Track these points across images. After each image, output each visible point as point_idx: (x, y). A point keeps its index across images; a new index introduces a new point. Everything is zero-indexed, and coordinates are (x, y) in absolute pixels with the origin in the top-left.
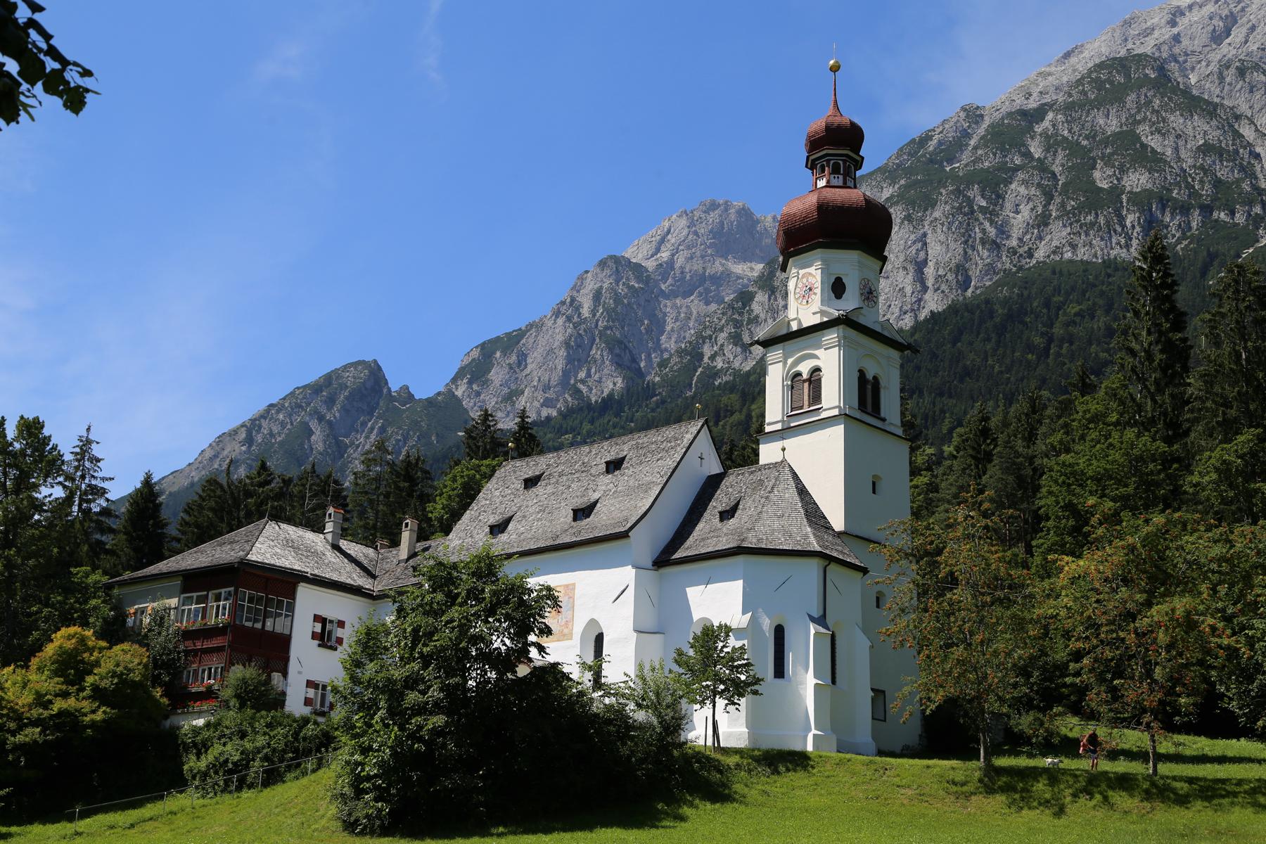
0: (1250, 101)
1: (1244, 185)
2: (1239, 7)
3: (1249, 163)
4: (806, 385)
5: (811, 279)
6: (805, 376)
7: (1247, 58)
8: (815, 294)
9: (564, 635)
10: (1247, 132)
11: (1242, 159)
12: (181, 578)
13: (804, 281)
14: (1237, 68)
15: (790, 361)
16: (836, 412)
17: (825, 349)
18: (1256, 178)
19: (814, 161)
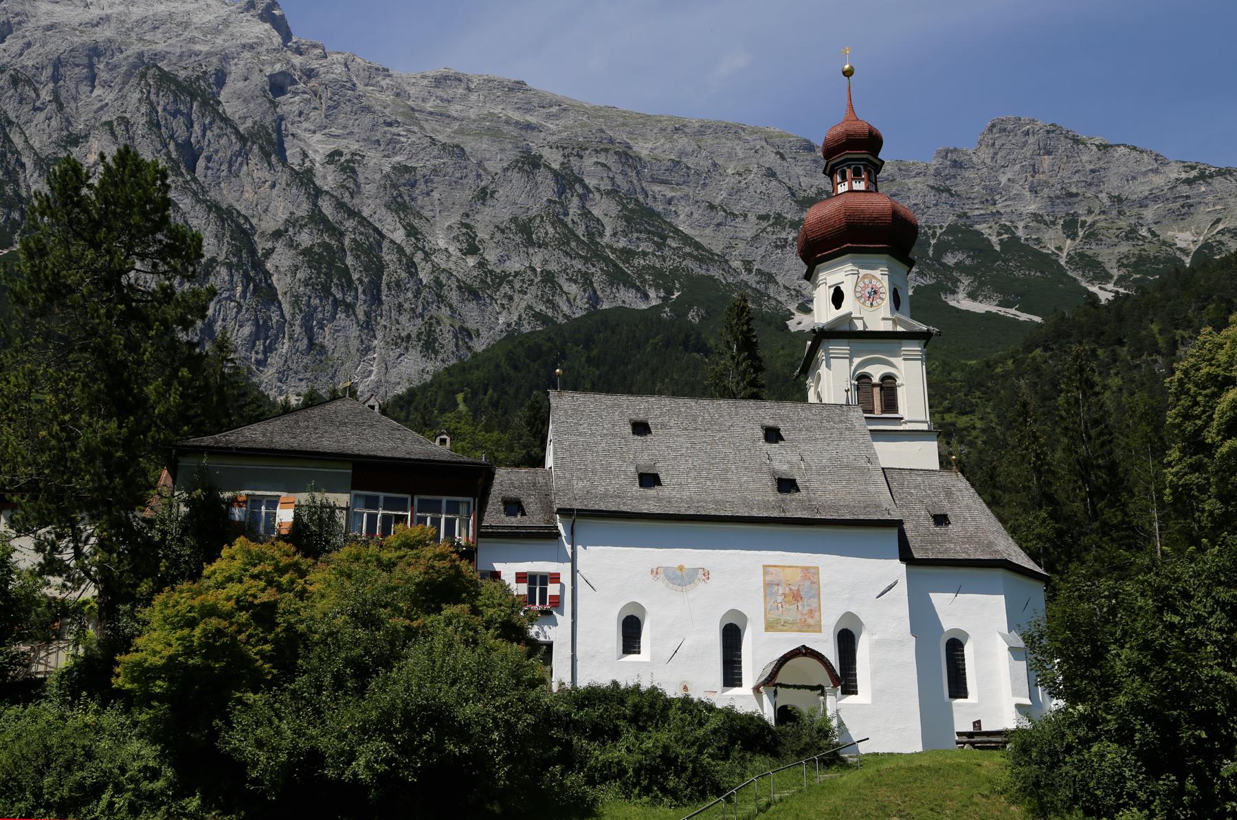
0: (18, 110)
1: (7, 188)
2: (17, 19)
3: (14, 169)
4: (877, 390)
5: (874, 282)
6: (876, 380)
7: (22, 70)
8: (883, 299)
9: (809, 626)
10: (17, 140)
11: (8, 163)
12: (351, 466)
13: (867, 281)
14: (11, 75)
15: (857, 361)
16: (925, 427)
17: (905, 359)
18: (18, 185)
19: (833, 166)
